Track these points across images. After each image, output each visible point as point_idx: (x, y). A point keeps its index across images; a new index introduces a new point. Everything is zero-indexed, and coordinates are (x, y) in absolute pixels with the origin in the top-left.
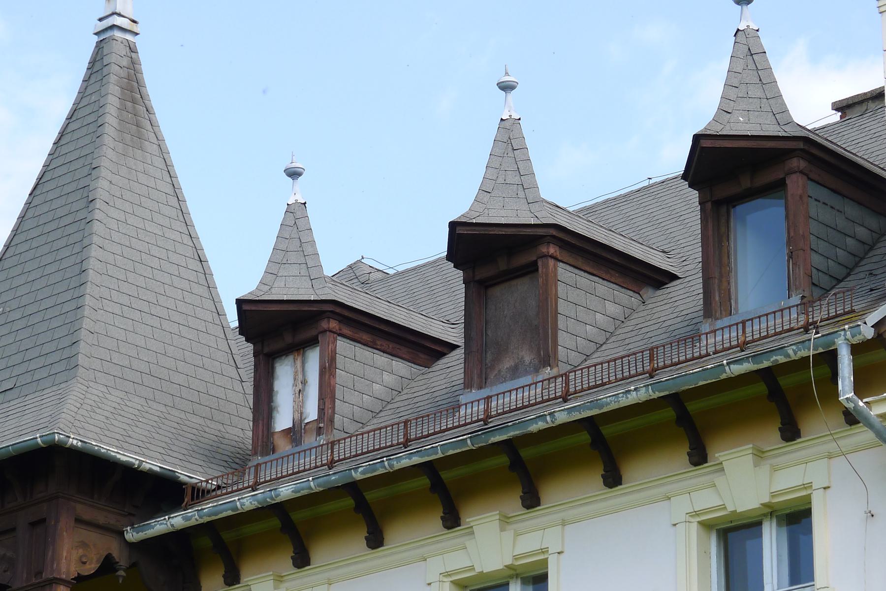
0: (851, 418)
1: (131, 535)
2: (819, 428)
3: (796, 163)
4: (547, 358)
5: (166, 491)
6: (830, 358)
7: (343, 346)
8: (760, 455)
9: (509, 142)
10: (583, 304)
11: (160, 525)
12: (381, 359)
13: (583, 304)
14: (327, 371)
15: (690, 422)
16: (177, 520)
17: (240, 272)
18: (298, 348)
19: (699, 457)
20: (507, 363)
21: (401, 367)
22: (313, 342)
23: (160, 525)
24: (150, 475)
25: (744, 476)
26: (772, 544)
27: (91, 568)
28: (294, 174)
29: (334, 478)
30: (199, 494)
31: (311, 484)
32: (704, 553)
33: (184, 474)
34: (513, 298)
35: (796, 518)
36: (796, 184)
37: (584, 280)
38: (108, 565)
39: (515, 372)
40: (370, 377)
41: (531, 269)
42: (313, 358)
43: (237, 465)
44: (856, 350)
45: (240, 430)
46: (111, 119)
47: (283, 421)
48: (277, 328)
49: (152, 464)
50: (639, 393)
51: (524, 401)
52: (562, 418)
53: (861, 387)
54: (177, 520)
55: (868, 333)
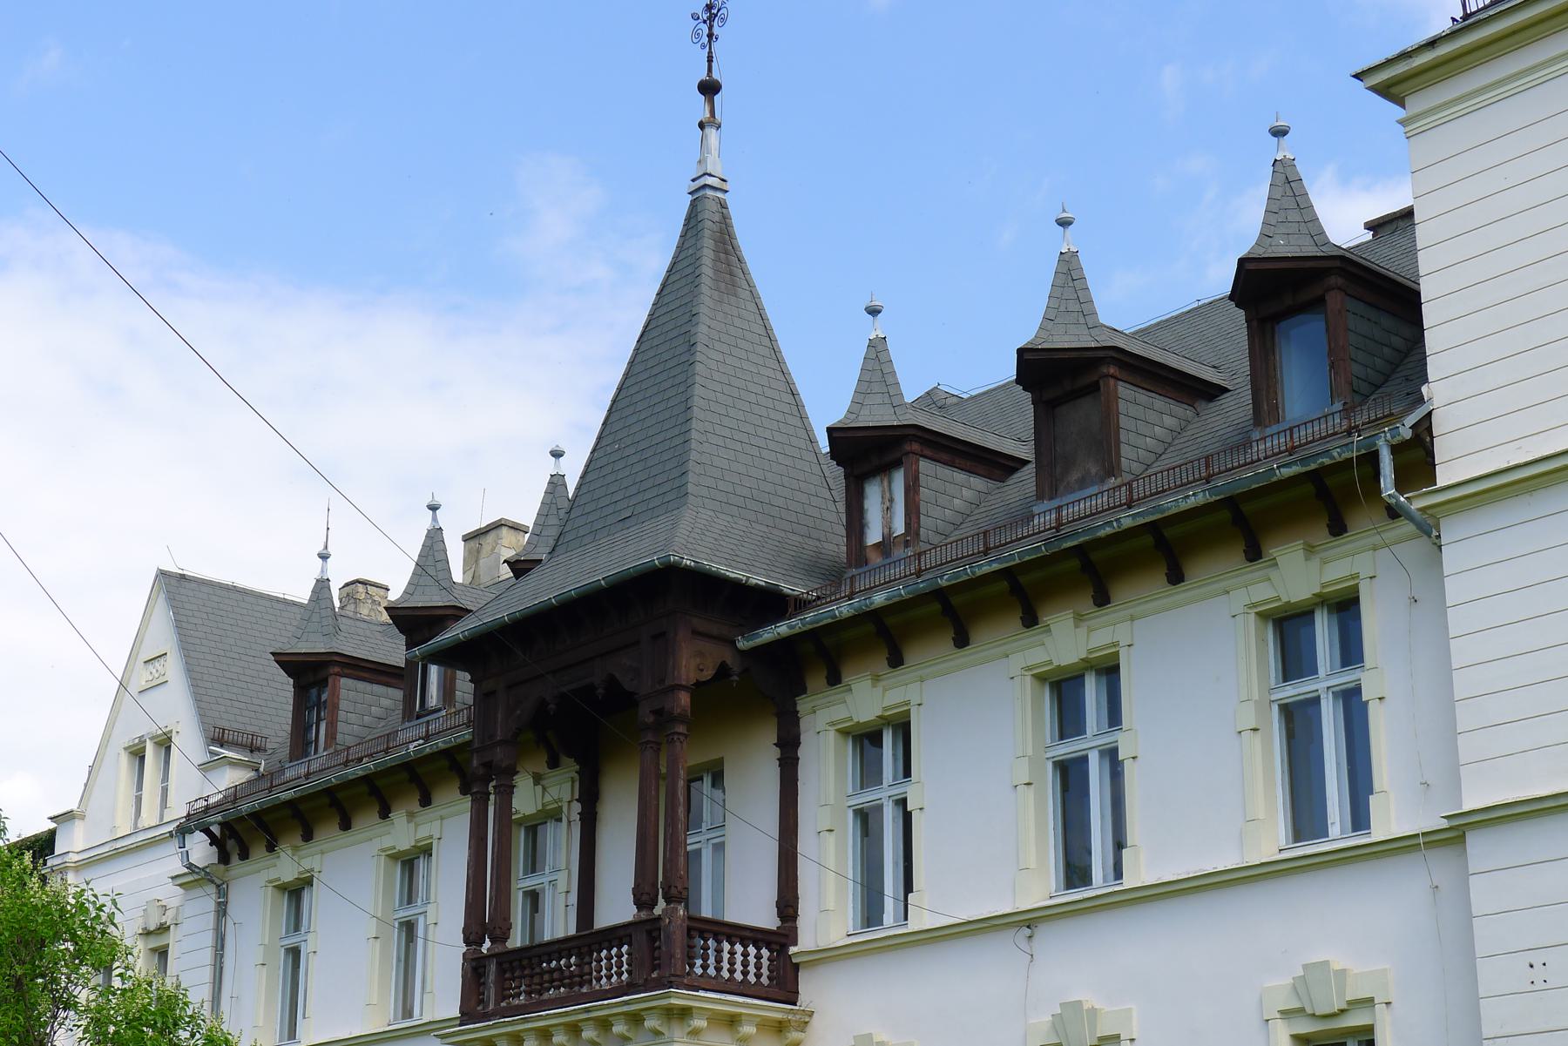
0: (1394, 513)
1: (742, 644)
2: (1365, 525)
3: (1334, 280)
4: (1112, 469)
5: (772, 603)
6: (1373, 458)
7: (924, 466)
8: (1310, 550)
9: (1069, 273)
10: (1144, 421)
11: (768, 634)
12: (960, 476)
13: (1144, 421)
14: (912, 490)
15: (1244, 523)
16: (782, 629)
17: (828, 403)
18: (884, 470)
19: (1254, 554)
20: (1075, 476)
21: (978, 483)
22: (897, 464)
23: (768, 634)
24: (757, 588)
25: (1296, 571)
26: (1324, 631)
27: (708, 674)
28: (874, 311)
29: (922, 585)
30: (801, 605)
31: (901, 591)
32: (1261, 640)
33: (786, 587)
34: (1078, 416)
35: (1345, 606)
36: (1334, 300)
37: (1142, 396)
38: (723, 671)
39: (1083, 483)
40: (951, 493)
41: (1094, 388)
42: (899, 479)
43: (834, 577)
44: (1396, 450)
45: (836, 546)
46: (707, 270)
47: (874, 536)
48: (865, 452)
49: (759, 580)
50: (1196, 498)
51: (1092, 509)
52: (1127, 523)
53: (1402, 484)
54: (782, 629)
55: (1406, 433)
